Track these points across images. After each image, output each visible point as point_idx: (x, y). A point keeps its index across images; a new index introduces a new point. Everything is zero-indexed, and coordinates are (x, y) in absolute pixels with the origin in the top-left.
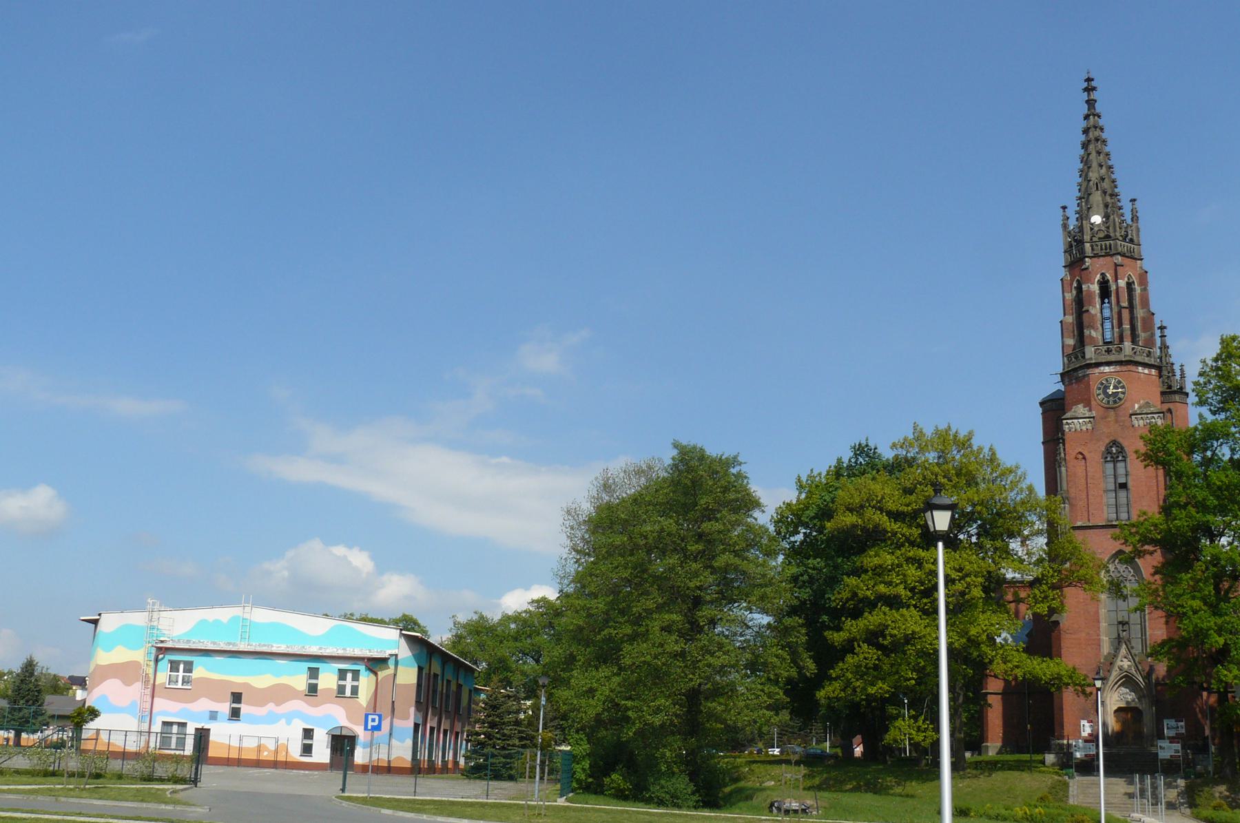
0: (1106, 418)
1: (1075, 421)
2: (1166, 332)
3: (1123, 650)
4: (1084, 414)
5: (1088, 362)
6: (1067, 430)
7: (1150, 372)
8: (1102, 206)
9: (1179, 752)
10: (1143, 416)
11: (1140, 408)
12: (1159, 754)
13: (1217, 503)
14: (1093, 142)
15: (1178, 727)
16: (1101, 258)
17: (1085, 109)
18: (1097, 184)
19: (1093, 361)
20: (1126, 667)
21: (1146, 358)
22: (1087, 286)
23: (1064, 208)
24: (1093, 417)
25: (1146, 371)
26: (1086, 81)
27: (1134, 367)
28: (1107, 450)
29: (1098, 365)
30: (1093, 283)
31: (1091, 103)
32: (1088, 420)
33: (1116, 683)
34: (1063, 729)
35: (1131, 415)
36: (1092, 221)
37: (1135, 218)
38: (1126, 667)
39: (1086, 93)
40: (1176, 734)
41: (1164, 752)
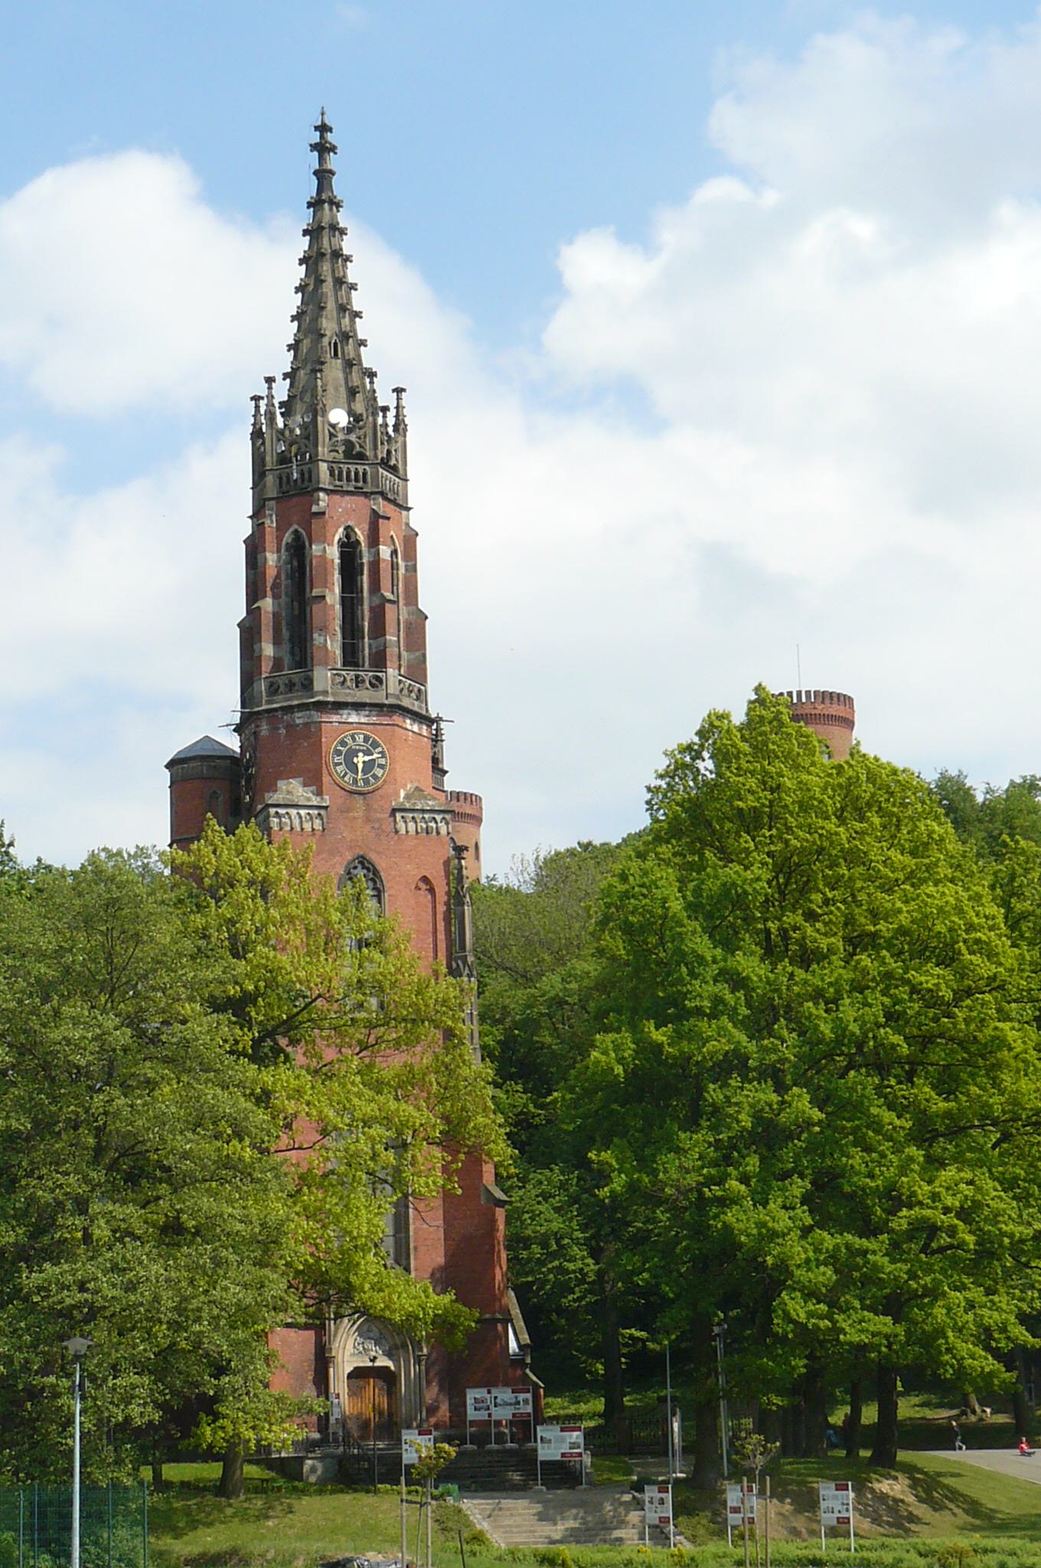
0: (349, 810)
1: (293, 812)
4: (309, 799)
5: (321, 698)
6: (276, 828)
7: (420, 729)
8: (343, 390)
9: (579, 1447)
10: (415, 815)
11: (408, 797)
12: (540, 1451)
13: (999, 1055)
14: (328, 256)
15: (518, 1403)
16: (347, 498)
17: (310, 188)
18: (336, 344)
19: (330, 699)
21: (416, 703)
22: (321, 547)
24: (326, 808)
25: (415, 728)
26: (317, 128)
27: (401, 719)
29: (338, 706)
30: (331, 544)
31: (323, 176)
32: (316, 812)
35: (394, 811)
36: (333, 421)
37: (402, 426)
39: (316, 154)
40: (514, 1415)
41: (549, 1448)
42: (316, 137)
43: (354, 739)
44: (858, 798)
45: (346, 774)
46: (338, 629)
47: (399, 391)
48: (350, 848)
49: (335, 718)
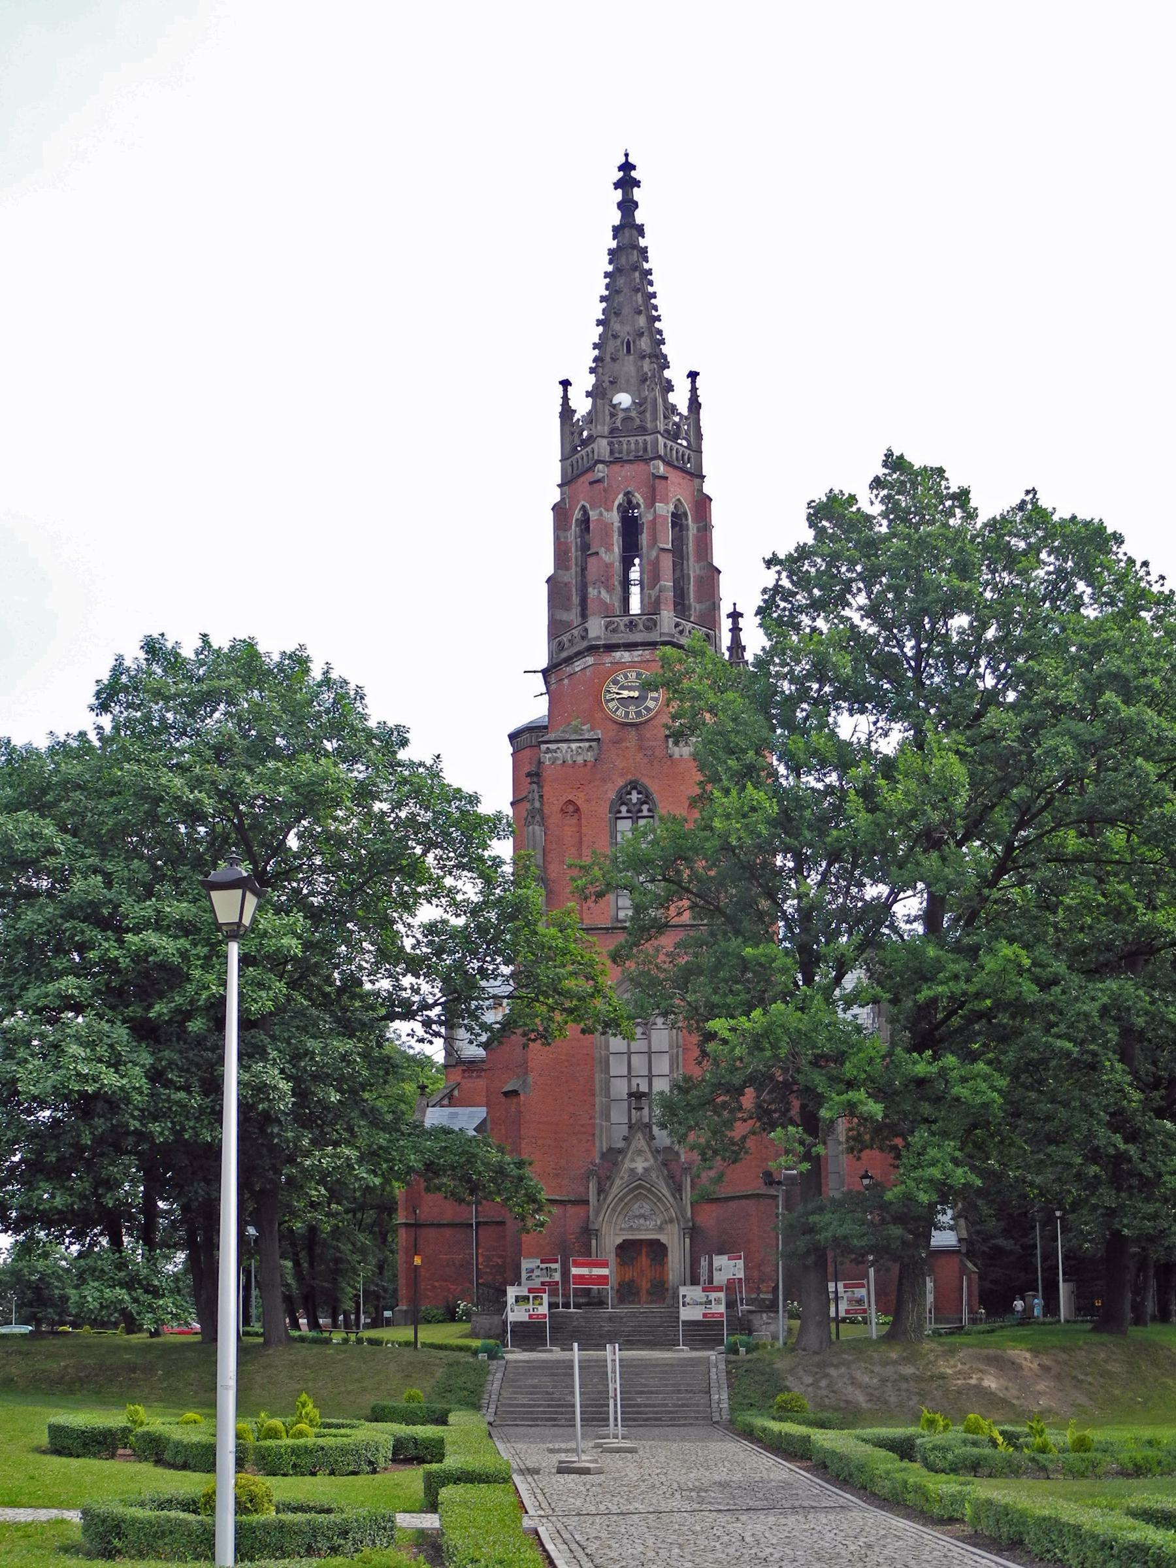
1: (564, 746)
2: (699, 381)
16: (627, 467)
17: (616, 217)
20: (640, 1170)
23: (566, 384)
29: (611, 648)
31: (628, 206)
32: (587, 744)
33: (621, 1199)
38: (640, 1170)
40: (705, 1315)
42: (637, 194)
43: (626, 677)
44: (1146, 1022)
45: (618, 709)
46: (616, 583)
47: (693, 375)
48: (622, 775)
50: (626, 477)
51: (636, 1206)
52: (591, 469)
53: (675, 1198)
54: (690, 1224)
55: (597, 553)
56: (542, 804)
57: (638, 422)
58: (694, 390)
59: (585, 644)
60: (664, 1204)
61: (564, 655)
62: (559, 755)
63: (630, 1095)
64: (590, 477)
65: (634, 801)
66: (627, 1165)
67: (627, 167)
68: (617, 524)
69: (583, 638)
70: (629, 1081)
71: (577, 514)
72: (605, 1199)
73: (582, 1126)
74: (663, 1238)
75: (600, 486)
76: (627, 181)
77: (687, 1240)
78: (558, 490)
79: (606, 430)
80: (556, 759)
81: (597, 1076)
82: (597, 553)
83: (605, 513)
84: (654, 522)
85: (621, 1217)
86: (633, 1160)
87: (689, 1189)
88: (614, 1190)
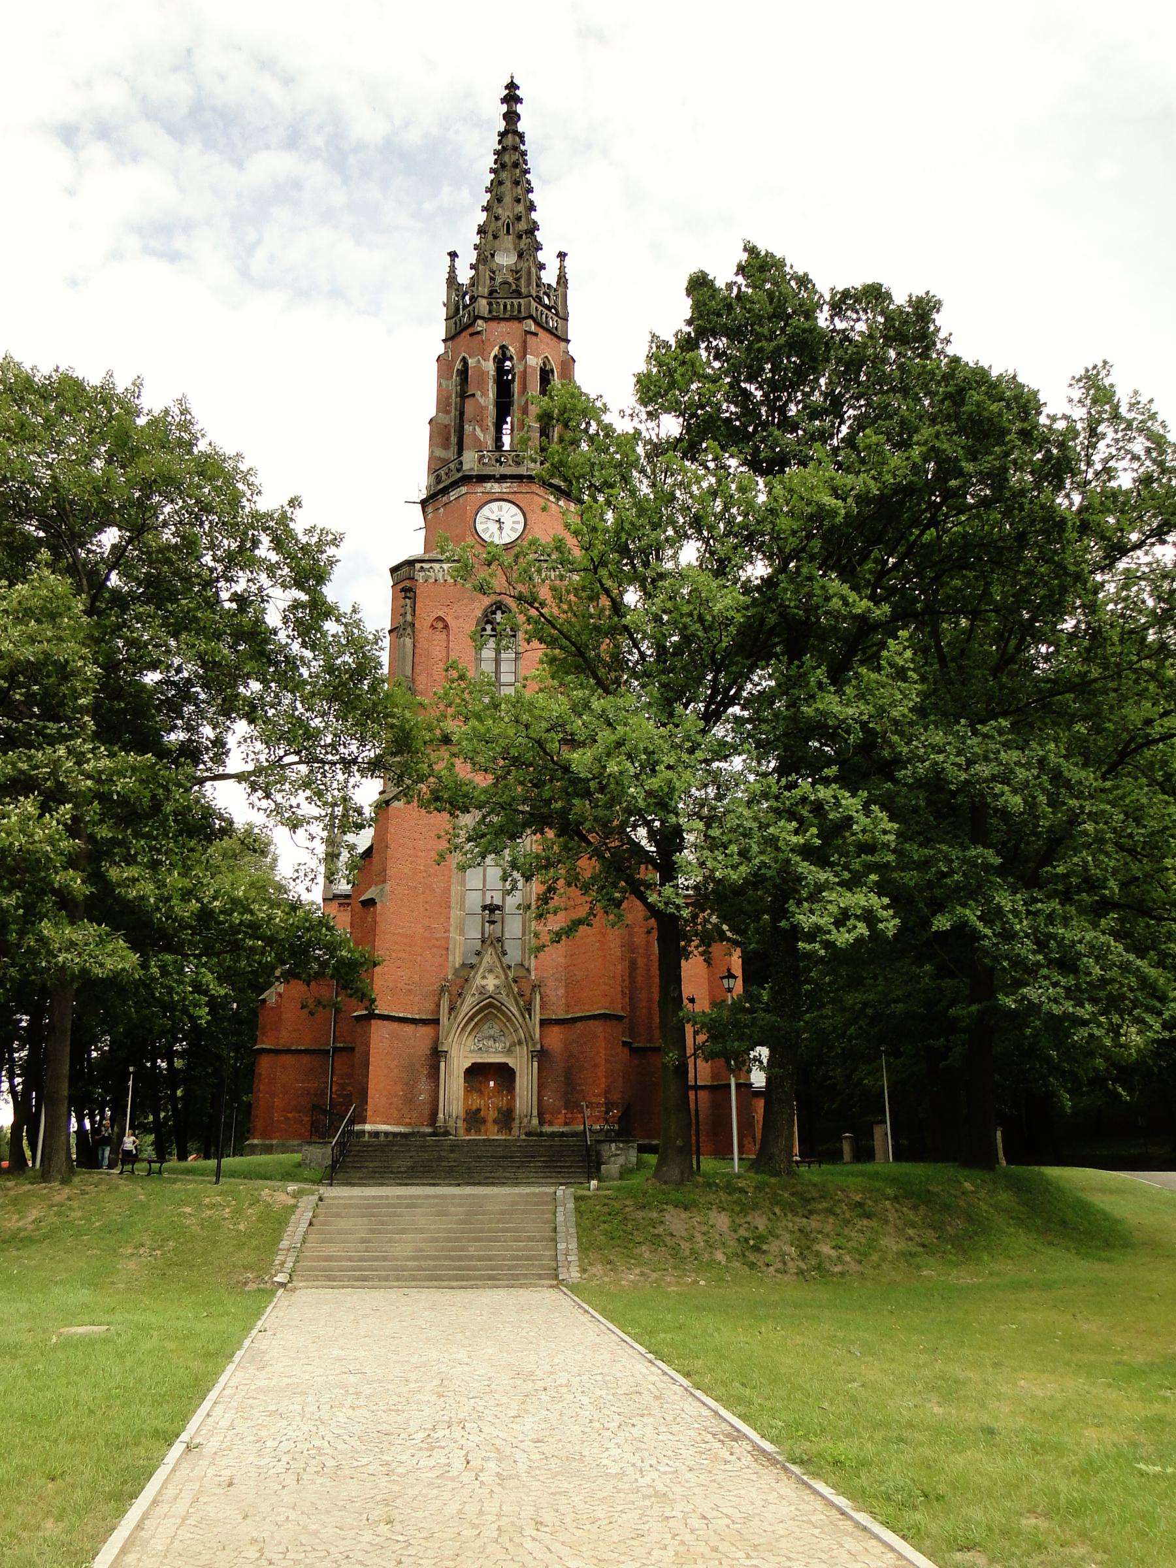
1: (436, 566)
3: (489, 958)
16: (503, 324)
17: (502, 125)
18: (508, 225)
20: (491, 988)
23: (453, 255)
28: (487, 616)
29: (482, 479)
31: (511, 117)
33: (471, 1019)
34: (367, 1103)
38: (491, 988)
42: (520, 108)
47: (562, 256)
49: (480, 490)
50: (500, 334)
51: (486, 1027)
52: (472, 324)
53: (524, 1018)
54: (538, 1047)
55: (473, 395)
56: (414, 615)
57: (514, 287)
58: (562, 268)
59: (460, 475)
60: (513, 1024)
61: (441, 486)
62: (432, 574)
63: (484, 908)
64: (471, 330)
65: (498, 620)
66: (479, 981)
67: (512, 86)
68: (492, 373)
69: (458, 470)
70: (484, 894)
71: (458, 365)
72: (455, 1018)
73: (437, 939)
74: (511, 1062)
75: (479, 337)
76: (512, 97)
77: (535, 1064)
78: (443, 345)
79: (486, 292)
80: (429, 577)
81: (453, 887)
82: (473, 395)
83: (482, 362)
84: (525, 371)
85: (471, 1037)
86: (484, 977)
87: (538, 1007)
88: (465, 1008)
